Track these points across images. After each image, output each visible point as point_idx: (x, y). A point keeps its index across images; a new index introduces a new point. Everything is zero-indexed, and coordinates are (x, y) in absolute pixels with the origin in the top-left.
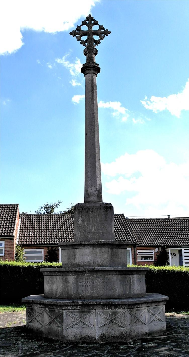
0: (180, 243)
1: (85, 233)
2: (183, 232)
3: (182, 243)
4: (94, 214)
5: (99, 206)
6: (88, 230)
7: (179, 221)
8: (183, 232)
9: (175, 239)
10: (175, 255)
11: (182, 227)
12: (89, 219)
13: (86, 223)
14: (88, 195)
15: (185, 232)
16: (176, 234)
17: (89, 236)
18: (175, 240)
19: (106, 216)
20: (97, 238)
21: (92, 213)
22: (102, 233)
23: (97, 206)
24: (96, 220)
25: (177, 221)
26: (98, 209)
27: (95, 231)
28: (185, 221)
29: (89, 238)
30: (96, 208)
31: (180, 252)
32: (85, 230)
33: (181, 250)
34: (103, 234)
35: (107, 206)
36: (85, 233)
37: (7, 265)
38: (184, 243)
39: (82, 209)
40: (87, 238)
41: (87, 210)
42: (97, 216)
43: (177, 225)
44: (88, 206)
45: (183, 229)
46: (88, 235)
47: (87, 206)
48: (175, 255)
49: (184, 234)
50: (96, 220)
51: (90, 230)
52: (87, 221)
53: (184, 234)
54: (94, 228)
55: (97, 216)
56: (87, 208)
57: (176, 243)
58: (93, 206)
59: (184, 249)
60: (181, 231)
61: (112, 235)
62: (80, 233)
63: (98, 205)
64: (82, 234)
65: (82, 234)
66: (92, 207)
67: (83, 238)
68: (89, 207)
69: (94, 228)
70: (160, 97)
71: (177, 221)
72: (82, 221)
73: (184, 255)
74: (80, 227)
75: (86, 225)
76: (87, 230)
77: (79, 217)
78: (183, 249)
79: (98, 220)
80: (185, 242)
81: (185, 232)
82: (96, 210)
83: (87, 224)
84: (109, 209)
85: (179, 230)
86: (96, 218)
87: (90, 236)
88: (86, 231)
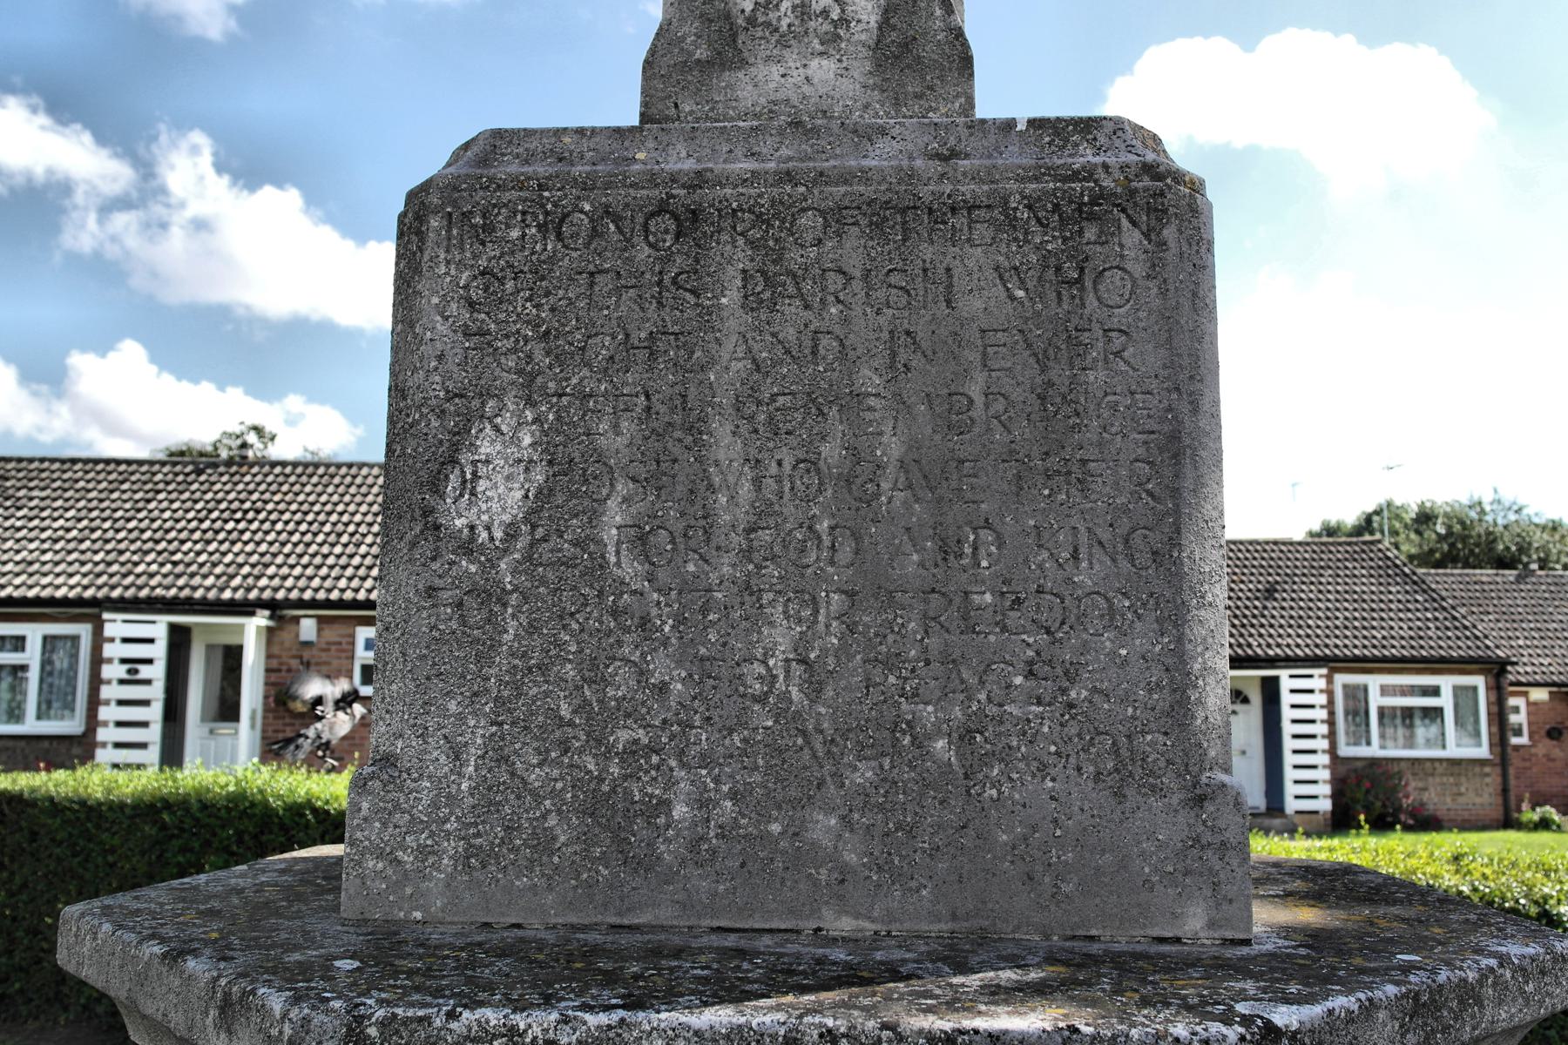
0: (1269, 646)
1: (597, 740)
2: (1275, 599)
3: (1279, 645)
4: (790, 333)
5: (911, 176)
6: (661, 667)
7: (1257, 551)
8: (1275, 599)
9: (1243, 626)
10: (1246, 700)
11: (1270, 575)
12: (696, 428)
13: (615, 516)
14: (706, 19)
15: (1284, 599)
16: (1247, 607)
17: (680, 811)
18: (1243, 631)
19: (1059, 373)
20: (851, 858)
21: (751, 301)
22: (965, 736)
23: (865, 176)
24: (831, 451)
25: (1248, 551)
26: (878, 226)
27: (815, 690)
28: (1282, 551)
29: (666, 852)
30: (836, 218)
31: (1271, 690)
32: (595, 674)
33: (1276, 679)
34: (986, 760)
35: (1088, 173)
36: (597, 740)
37: (315, 810)
38: (1288, 646)
39: (554, 225)
40: (620, 842)
41: (643, 252)
42: (869, 379)
43: (1245, 566)
44: (690, 165)
45: (1277, 582)
46: (643, 789)
47: (652, 179)
48: (1246, 700)
49: (1283, 608)
50: (831, 451)
51: (703, 670)
52: (654, 480)
53: (1283, 608)
54: (780, 637)
55: (869, 379)
56: (662, 209)
57: (1249, 646)
58: (788, 177)
59: (1291, 676)
60: (1270, 592)
61: (1200, 800)
62: (477, 734)
63: (884, 146)
64: (527, 755)
65: (527, 755)
66: (764, 195)
67: (544, 843)
68: (699, 180)
69: (780, 637)
70: (1159, 42)
71: (1248, 551)
72: (539, 477)
73: (1287, 699)
74: (490, 595)
75: (630, 569)
76: (642, 674)
77: (484, 394)
78: (1284, 674)
79: (892, 447)
80: (1290, 641)
81: (1284, 599)
82: (852, 250)
83: (640, 539)
84: (1132, 237)
85: (1258, 590)
86: (836, 424)
87: (703, 803)
88: (622, 683)
